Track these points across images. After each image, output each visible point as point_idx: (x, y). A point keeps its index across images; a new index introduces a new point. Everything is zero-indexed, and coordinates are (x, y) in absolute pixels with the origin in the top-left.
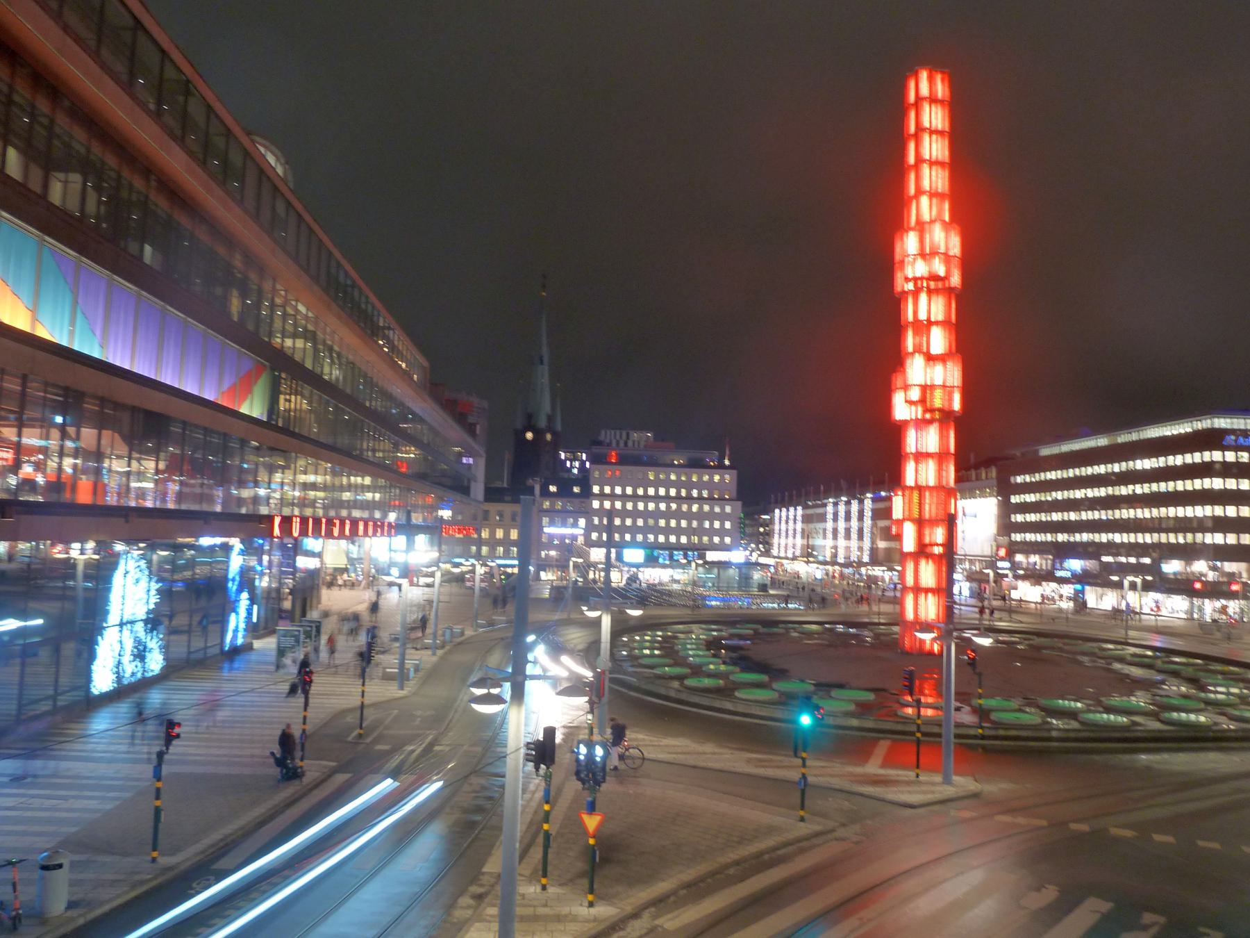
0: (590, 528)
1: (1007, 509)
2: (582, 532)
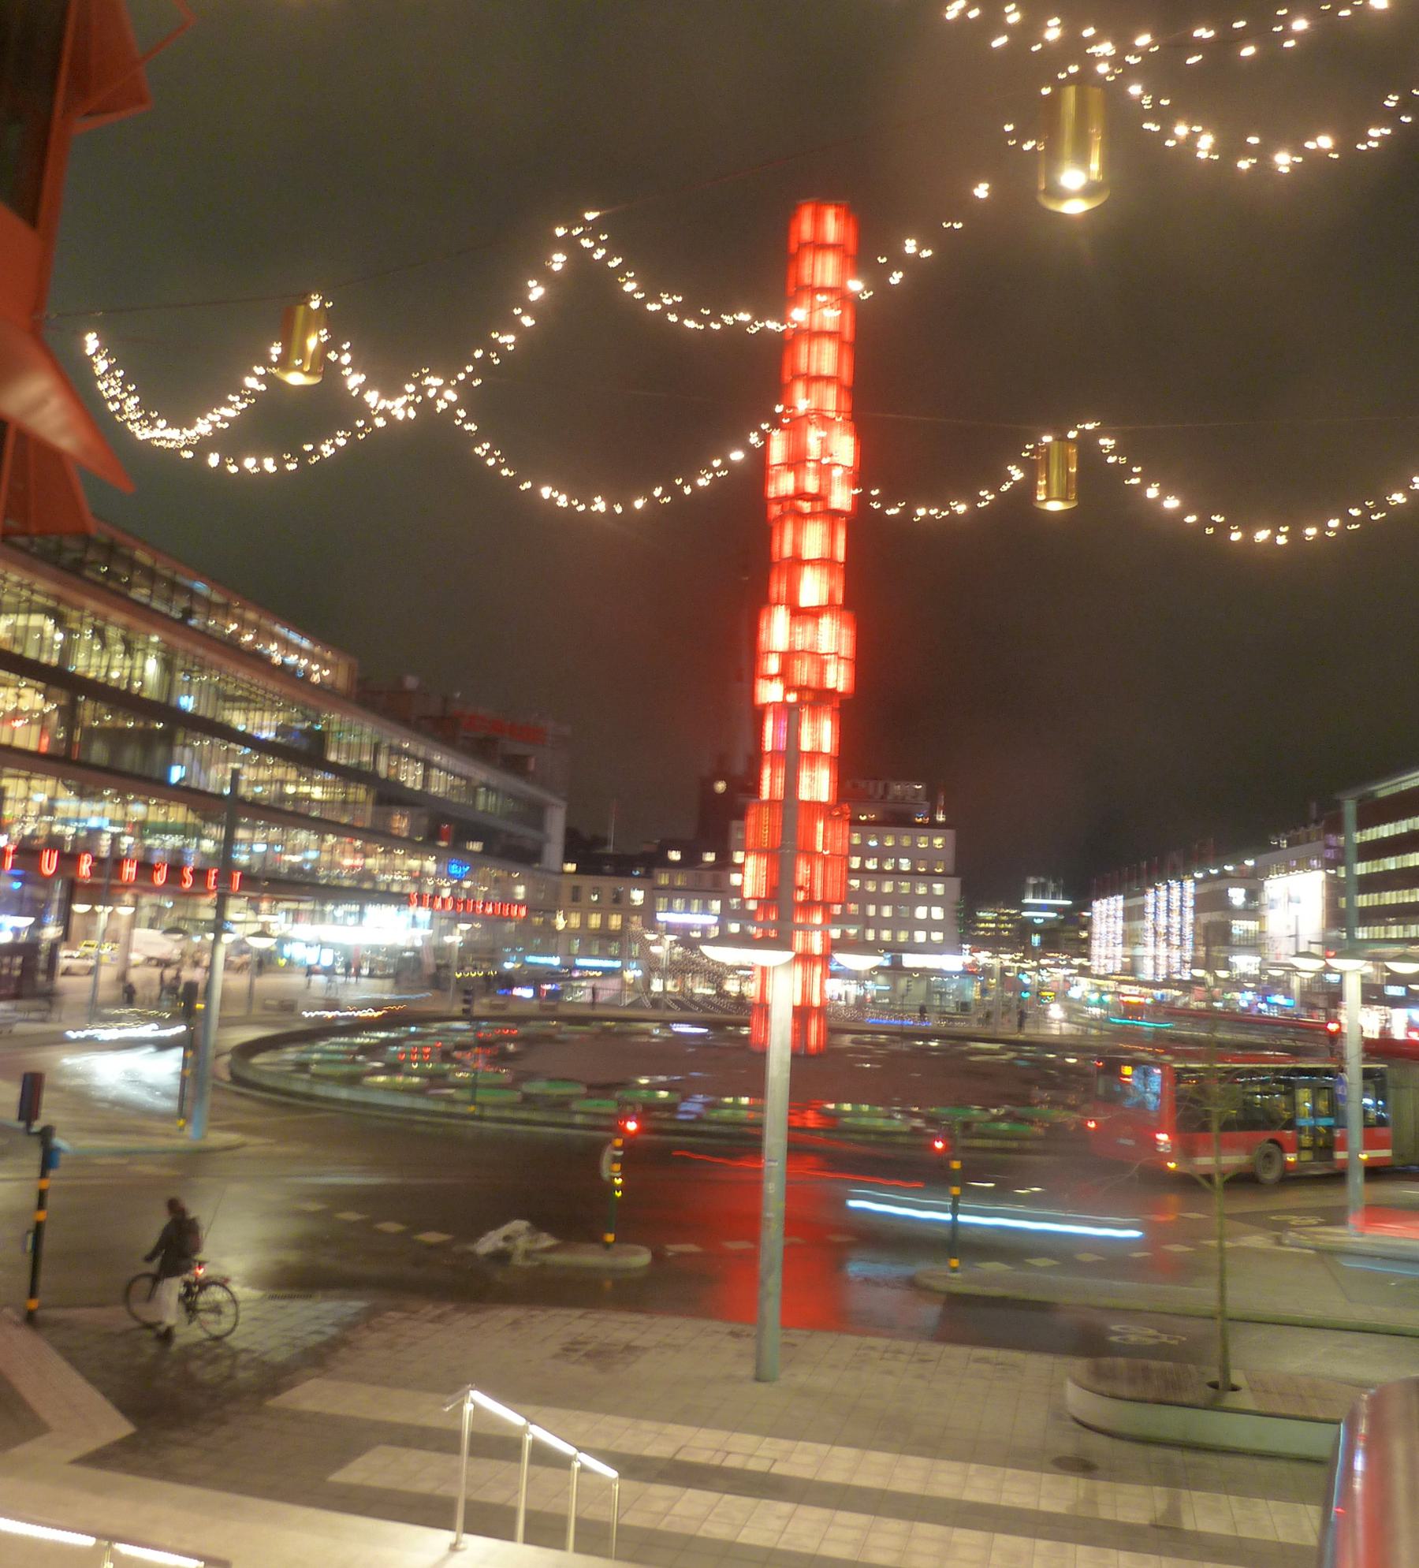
0: (726, 915)
1: (1335, 888)
2: (715, 920)
